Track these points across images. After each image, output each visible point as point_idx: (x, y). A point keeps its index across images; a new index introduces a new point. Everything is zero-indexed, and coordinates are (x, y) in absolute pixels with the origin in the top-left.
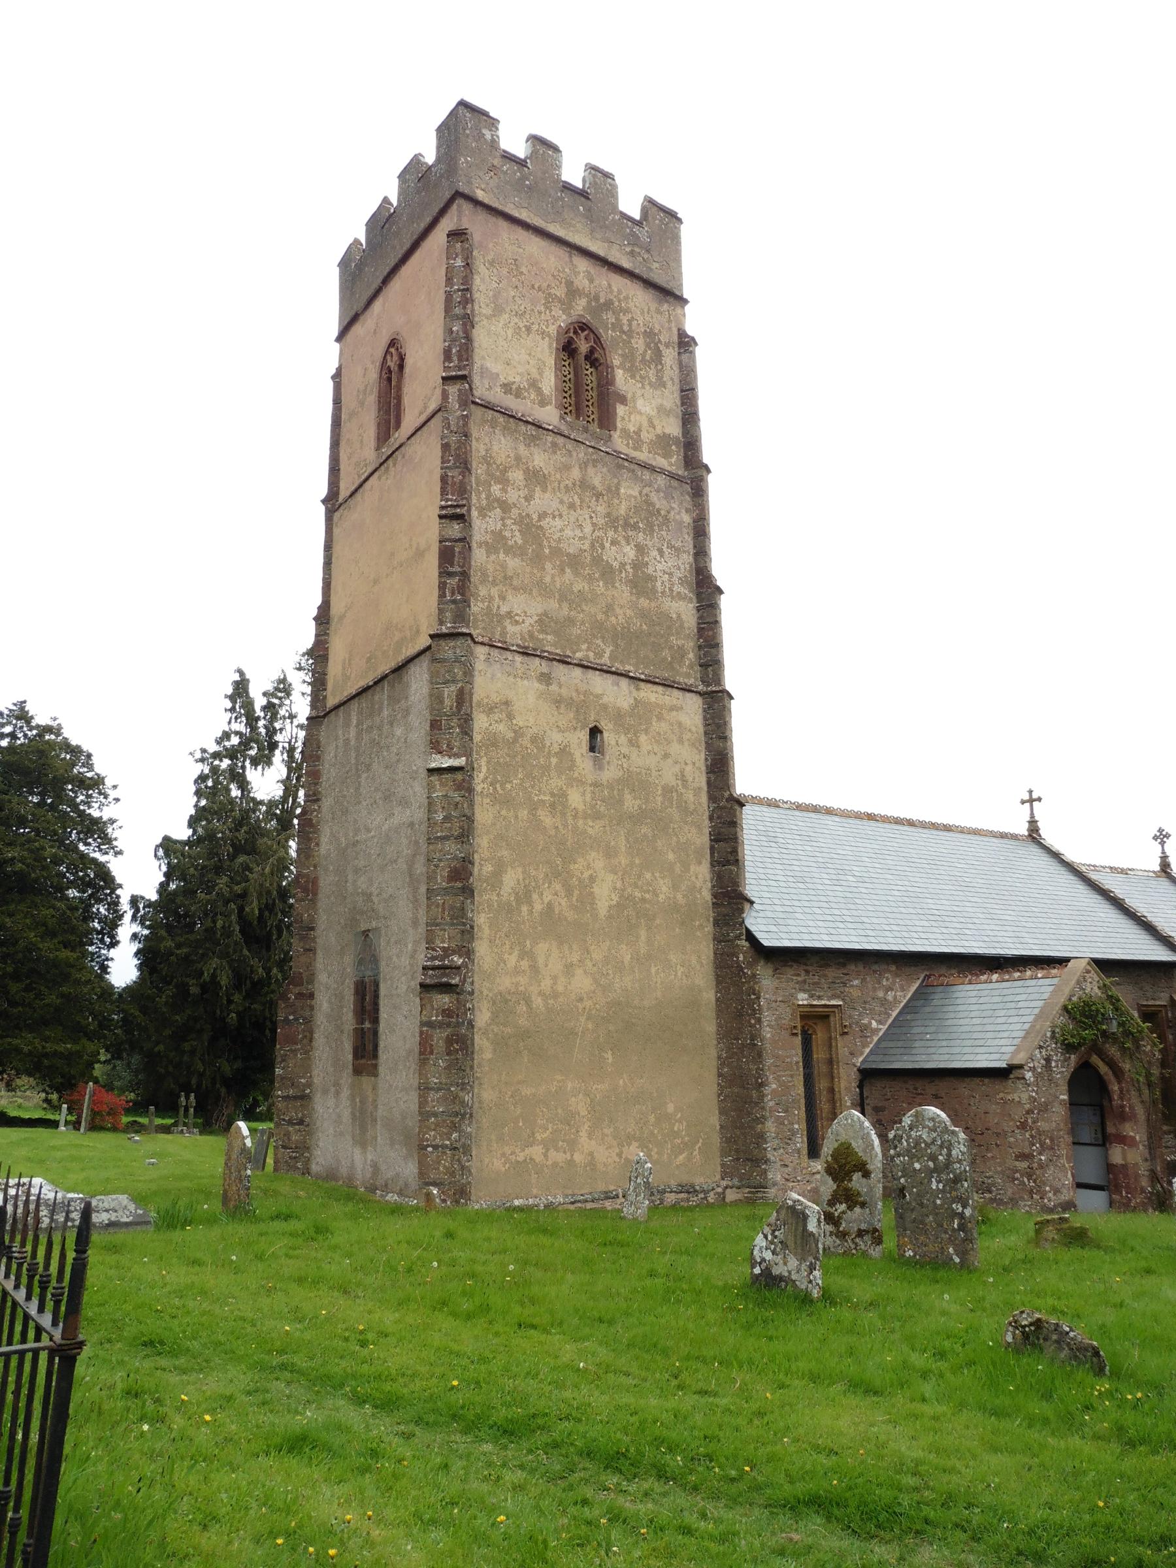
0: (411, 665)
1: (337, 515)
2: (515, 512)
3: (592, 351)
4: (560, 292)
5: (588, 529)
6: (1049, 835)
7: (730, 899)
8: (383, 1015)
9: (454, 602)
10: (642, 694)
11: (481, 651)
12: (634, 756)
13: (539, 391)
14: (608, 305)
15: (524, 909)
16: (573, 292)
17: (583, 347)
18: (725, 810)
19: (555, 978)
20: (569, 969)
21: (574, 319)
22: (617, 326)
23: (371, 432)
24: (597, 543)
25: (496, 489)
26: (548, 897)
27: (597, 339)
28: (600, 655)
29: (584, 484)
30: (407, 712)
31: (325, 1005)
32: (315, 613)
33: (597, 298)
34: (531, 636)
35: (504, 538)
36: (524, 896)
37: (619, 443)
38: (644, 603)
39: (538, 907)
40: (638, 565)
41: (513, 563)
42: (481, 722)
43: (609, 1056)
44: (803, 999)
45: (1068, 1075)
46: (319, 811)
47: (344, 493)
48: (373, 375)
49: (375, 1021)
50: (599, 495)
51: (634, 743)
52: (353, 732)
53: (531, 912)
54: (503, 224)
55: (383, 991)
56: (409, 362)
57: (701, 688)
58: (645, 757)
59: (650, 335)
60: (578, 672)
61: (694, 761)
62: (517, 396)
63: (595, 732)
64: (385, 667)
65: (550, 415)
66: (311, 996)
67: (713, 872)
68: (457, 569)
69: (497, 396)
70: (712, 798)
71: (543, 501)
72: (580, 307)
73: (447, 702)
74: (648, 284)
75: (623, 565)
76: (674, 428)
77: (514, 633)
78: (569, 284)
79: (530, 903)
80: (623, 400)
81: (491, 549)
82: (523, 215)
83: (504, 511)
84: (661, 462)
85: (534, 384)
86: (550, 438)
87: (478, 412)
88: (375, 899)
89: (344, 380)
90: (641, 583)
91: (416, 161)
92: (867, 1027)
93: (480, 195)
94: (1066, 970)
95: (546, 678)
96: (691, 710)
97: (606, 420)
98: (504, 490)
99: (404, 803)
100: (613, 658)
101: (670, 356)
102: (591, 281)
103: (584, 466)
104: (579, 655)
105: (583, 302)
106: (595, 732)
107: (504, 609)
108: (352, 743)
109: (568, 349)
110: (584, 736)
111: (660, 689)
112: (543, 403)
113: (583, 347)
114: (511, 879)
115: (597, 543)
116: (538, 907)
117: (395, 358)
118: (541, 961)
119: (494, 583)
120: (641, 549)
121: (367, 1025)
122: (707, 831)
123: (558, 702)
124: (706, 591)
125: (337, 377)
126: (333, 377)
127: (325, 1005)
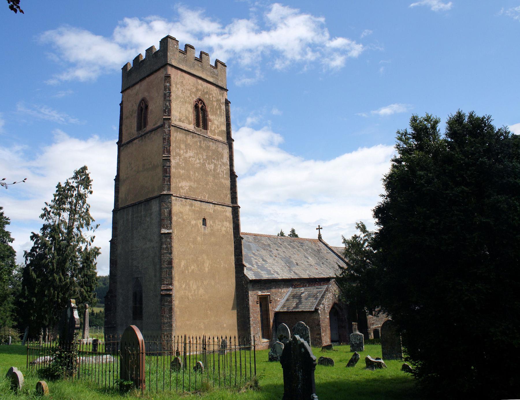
0: (153, 200)
1: (122, 148)
2: (182, 157)
3: (202, 106)
4: (194, 90)
5: (201, 161)
6: (324, 238)
7: (239, 266)
8: (144, 302)
9: (167, 184)
10: (216, 208)
11: (173, 198)
12: (214, 226)
13: (189, 121)
14: (207, 93)
15: (187, 272)
16: (197, 90)
17: (200, 106)
18: (238, 238)
19: (195, 290)
20: (198, 288)
21: (198, 98)
22: (209, 99)
23: (135, 125)
24: (204, 164)
25: (178, 150)
26: (192, 267)
27: (204, 104)
28: (205, 197)
29: (201, 147)
30: (151, 214)
31: (121, 299)
32: (115, 178)
33: (204, 91)
34: (187, 193)
35: (180, 165)
36: (187, 267)
37: (209, 134)
38: (216, 181)
39: (190, 271)
40: (215, 170)
41: (182, 172)
42: (174, 218)
43: (209, 312)
44: (260, 293)
45: (329, 311)
46: (117, 240)
47: (124, 141)
48: (136, 108)
49: (141, 304)
50: (204, 150)
51: (214, 222)
52: (130, 217)
53: (188, 272)
54: (179, 72)
55: (144, 295)
56: (150, 108)
57: (231, 205)
58: (217, 226)
59: (218, 101)
60: (199, 202)
61: (229, 226)
62: (183, 122)
63: (204, 220)
64: (142, 199)
65: (191, 127)
66: (116, 296)
67: (235, 258)
68: (168, 175)
69: (177, 123)
70: (235, 237)
71: (190, 154)
72: (199, 95)
73: (166, 214)
74: (217, 86)
75: (211, 170)
76: (224, 128)
77: (183, 193)
78: (196, 88)
79: (188, 270)
80: (211, 121)
81: (176, 169)
82: (185, 68)
83: (180, 157)
84: (220, 138)
85: (187, 118)
86: (192, 134)
87: (172, 127)
88: (140, 268)
89: (124, 105)
90: (216, 176)
91: (151, 48)
92: (277, 300)
93: (174, 64)
94: (397, 116)
95: (191, 205)
96: (229, 211)
97: (205, 127)
98: (180, 151)
99: (151, 241)
100: (208, 198)
101: (223, 107)
102: (202, 86)
103: (200, 142)
104: (199, 198)
105: (200, 93)
106: (204, 220)
107: (180, 185)
108: (130, 220)
109: (196, 107)
110: (201, 221)
111: (221, 206)
112: (190, 124)
113: (200, 106)
114: (183, 263)
115: (204, 164)
116: (190, 271)
117: (144, 105)
118: (191, 286)
119: (177, 178)
120: (216, 165)
121: (138, 305)
122: (233, 246)
123: (194, 211)
124: (233, 177)
125: (121, 104)
126: (120, 104)
127: (121, 299)
